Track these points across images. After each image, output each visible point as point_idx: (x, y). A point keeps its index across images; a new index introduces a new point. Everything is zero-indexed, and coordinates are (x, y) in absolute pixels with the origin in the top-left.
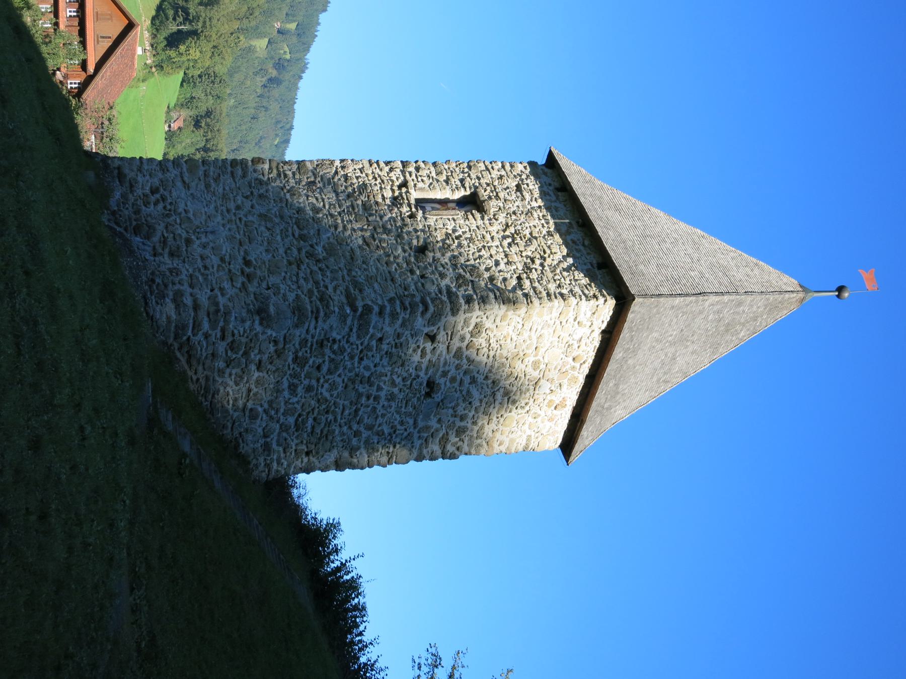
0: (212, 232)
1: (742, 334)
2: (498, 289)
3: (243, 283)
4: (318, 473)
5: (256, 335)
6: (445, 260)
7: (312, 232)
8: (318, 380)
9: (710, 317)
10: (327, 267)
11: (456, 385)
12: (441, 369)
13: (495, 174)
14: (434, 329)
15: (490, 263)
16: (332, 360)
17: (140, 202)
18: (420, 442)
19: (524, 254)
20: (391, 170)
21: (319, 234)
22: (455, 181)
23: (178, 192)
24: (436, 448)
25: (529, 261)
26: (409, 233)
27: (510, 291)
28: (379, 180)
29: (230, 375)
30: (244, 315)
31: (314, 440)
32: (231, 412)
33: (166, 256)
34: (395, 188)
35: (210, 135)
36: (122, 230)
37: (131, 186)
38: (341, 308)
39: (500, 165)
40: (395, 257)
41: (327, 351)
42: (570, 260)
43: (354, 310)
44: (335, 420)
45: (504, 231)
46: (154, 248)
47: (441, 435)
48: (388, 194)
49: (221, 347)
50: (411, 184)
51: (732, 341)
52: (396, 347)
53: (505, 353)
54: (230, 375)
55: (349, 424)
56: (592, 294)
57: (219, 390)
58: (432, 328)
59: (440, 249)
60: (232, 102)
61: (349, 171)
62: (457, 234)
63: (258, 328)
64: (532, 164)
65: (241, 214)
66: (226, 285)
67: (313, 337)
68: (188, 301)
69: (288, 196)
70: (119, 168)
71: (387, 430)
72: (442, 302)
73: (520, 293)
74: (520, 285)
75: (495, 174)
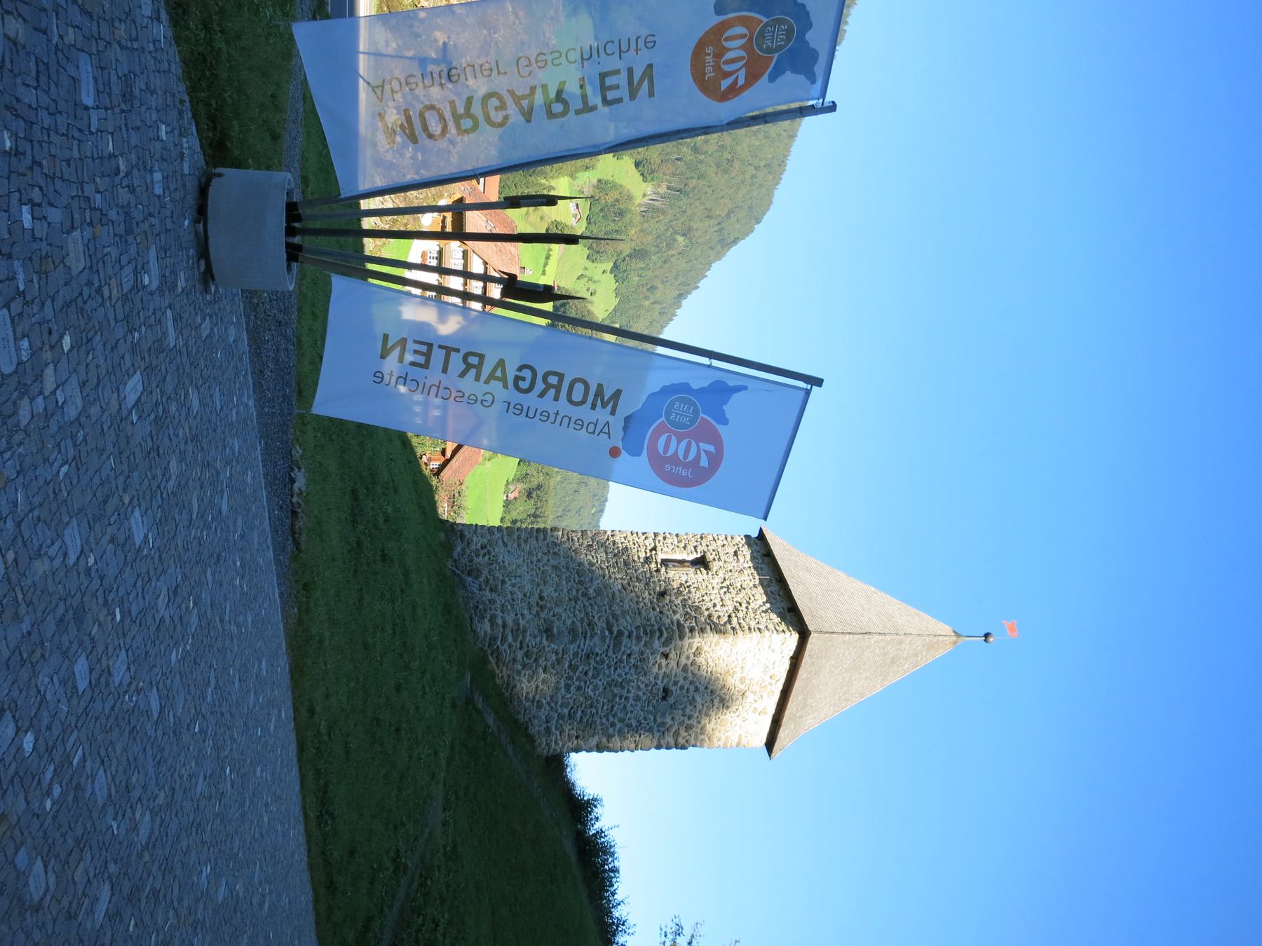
0: (519, 576)
1: (906, 666)
2: (714, 623)
3: (537, 612)
4: (584, 753)
5: (544, 647)
6: (678, 602)
7: (587, 580)
8: (585, 683)
9: (877, 652)
10: (595, 603)
11: (684, 692)
12: (673, 679)
13: (720, 543)
14: (667, 649)
15: (710, 605)
16: (595, 668)
17: (473, 554)
18: (658, 734)
19: (735, 600)
20: (646, 538)
21: (592, 581)
22: (690, 547)
23: (499, 549)
24: (671, 741)
25: (738, 604)
26: (654, 582)
27: (722, 625)
28: (637, 545)
29: (525, 675)
30: (536, 632)
31: (582, 727)
32: (524, 702)
33: (487, 591)
34: (648, 551)
35: (539, 505)
36: (460, 572)
37: (469, 543)
38: (602, 631)
39: (724, 537)
40: (643, 598)
41: (592, 662)
42: (768, 605)
43: (611, 632)
44: (597, 713)
45: (722, 583)
46: (480, 585)
47: (674, 730)
48: (642, 555)
49: (520, 654)
50: (659, 549)
51: (898, 671)
52: (640, 661)
53: (719, 670)
54: (525, 675)
55: (607, 716)
56: (781, 629)
57: (516, 686)
58: (666, 649)
59: (675, 594)
60: (559, 478)
61: (617, 539)
62: (688, 584)
64: (747, 537)
65: (540, 565)
66: (526, 612)
67: (582, 651)
68: (500, 621)
69: (573, 553)
70: (461, 531)
71: (634, 724)
72: (673, 630)
73: (729, 626)
74: (729, 621)
75: (720, 543)
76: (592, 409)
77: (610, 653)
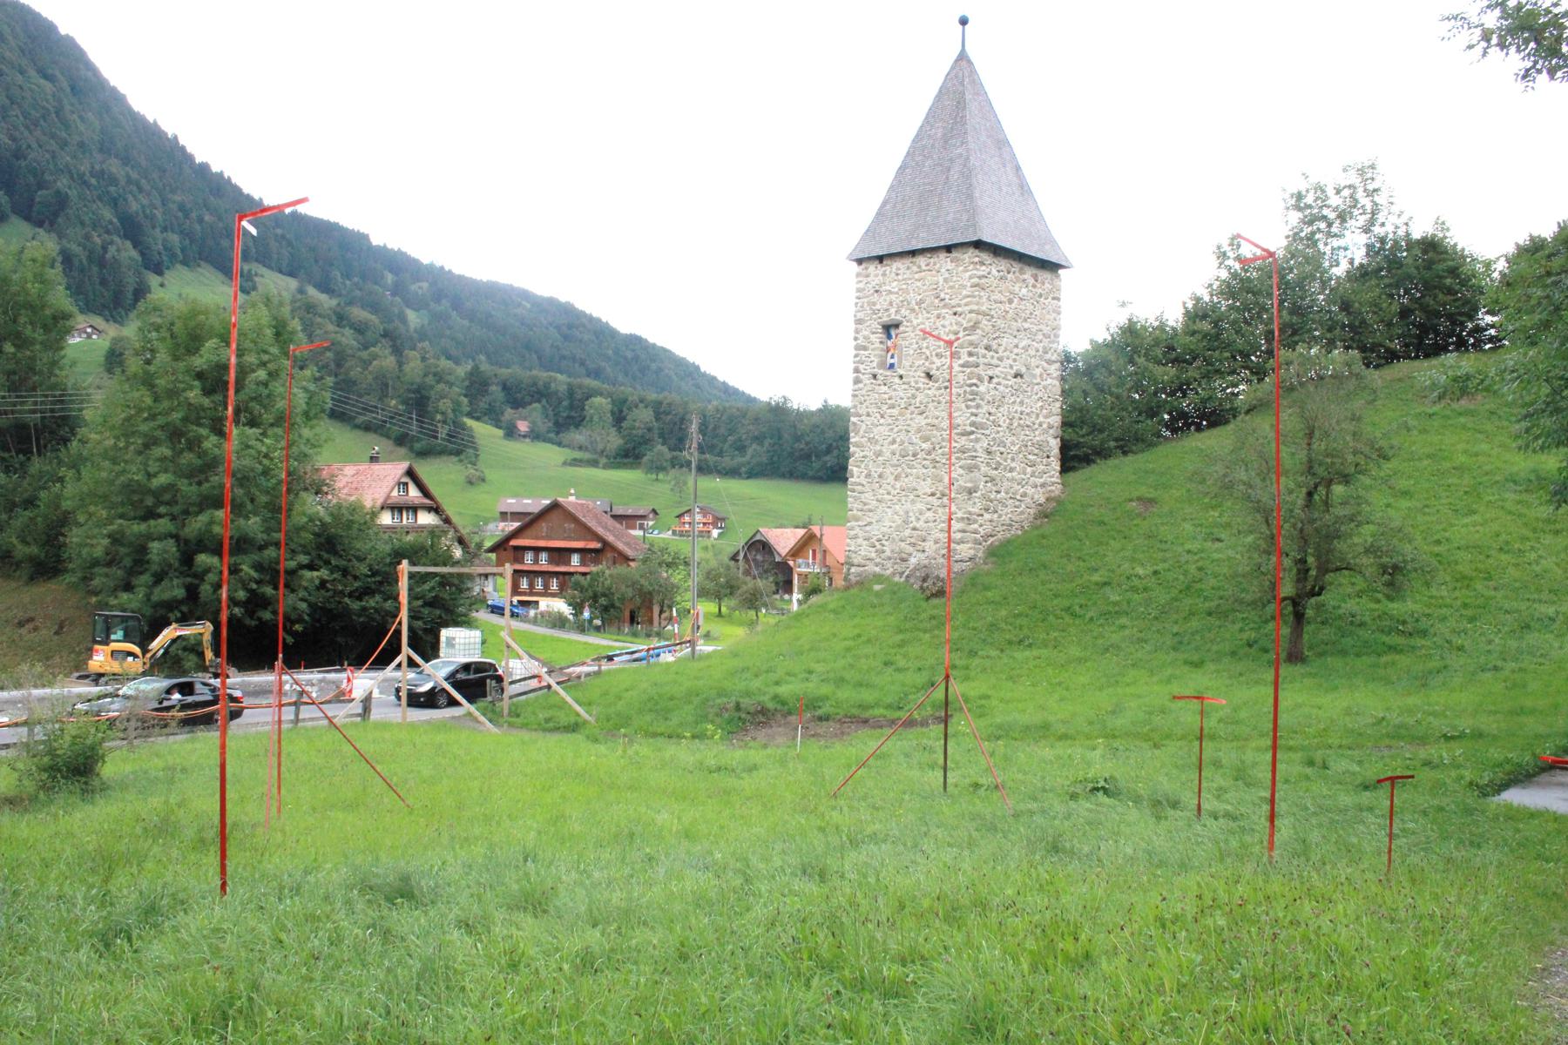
43: (973, 433)
49: (987, 516)
55: (1034, 431)
63: (978, 494)
76: (837, 474)
77: (987, 432)
